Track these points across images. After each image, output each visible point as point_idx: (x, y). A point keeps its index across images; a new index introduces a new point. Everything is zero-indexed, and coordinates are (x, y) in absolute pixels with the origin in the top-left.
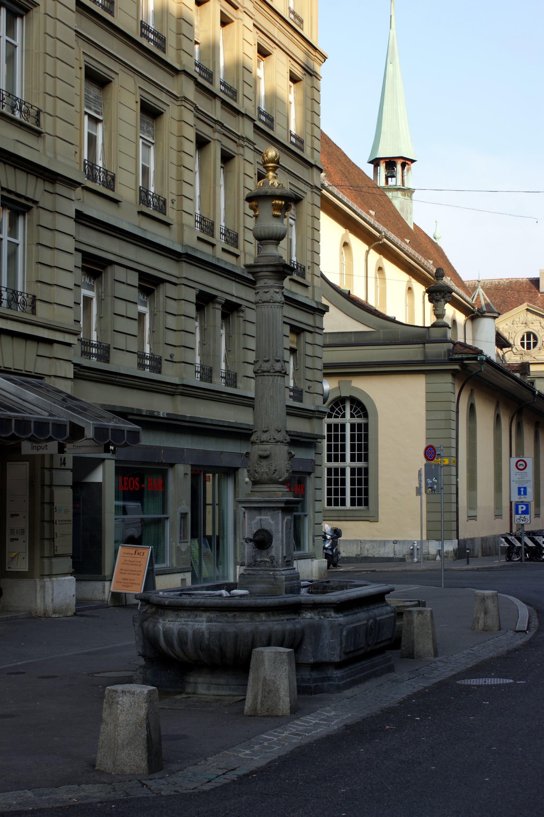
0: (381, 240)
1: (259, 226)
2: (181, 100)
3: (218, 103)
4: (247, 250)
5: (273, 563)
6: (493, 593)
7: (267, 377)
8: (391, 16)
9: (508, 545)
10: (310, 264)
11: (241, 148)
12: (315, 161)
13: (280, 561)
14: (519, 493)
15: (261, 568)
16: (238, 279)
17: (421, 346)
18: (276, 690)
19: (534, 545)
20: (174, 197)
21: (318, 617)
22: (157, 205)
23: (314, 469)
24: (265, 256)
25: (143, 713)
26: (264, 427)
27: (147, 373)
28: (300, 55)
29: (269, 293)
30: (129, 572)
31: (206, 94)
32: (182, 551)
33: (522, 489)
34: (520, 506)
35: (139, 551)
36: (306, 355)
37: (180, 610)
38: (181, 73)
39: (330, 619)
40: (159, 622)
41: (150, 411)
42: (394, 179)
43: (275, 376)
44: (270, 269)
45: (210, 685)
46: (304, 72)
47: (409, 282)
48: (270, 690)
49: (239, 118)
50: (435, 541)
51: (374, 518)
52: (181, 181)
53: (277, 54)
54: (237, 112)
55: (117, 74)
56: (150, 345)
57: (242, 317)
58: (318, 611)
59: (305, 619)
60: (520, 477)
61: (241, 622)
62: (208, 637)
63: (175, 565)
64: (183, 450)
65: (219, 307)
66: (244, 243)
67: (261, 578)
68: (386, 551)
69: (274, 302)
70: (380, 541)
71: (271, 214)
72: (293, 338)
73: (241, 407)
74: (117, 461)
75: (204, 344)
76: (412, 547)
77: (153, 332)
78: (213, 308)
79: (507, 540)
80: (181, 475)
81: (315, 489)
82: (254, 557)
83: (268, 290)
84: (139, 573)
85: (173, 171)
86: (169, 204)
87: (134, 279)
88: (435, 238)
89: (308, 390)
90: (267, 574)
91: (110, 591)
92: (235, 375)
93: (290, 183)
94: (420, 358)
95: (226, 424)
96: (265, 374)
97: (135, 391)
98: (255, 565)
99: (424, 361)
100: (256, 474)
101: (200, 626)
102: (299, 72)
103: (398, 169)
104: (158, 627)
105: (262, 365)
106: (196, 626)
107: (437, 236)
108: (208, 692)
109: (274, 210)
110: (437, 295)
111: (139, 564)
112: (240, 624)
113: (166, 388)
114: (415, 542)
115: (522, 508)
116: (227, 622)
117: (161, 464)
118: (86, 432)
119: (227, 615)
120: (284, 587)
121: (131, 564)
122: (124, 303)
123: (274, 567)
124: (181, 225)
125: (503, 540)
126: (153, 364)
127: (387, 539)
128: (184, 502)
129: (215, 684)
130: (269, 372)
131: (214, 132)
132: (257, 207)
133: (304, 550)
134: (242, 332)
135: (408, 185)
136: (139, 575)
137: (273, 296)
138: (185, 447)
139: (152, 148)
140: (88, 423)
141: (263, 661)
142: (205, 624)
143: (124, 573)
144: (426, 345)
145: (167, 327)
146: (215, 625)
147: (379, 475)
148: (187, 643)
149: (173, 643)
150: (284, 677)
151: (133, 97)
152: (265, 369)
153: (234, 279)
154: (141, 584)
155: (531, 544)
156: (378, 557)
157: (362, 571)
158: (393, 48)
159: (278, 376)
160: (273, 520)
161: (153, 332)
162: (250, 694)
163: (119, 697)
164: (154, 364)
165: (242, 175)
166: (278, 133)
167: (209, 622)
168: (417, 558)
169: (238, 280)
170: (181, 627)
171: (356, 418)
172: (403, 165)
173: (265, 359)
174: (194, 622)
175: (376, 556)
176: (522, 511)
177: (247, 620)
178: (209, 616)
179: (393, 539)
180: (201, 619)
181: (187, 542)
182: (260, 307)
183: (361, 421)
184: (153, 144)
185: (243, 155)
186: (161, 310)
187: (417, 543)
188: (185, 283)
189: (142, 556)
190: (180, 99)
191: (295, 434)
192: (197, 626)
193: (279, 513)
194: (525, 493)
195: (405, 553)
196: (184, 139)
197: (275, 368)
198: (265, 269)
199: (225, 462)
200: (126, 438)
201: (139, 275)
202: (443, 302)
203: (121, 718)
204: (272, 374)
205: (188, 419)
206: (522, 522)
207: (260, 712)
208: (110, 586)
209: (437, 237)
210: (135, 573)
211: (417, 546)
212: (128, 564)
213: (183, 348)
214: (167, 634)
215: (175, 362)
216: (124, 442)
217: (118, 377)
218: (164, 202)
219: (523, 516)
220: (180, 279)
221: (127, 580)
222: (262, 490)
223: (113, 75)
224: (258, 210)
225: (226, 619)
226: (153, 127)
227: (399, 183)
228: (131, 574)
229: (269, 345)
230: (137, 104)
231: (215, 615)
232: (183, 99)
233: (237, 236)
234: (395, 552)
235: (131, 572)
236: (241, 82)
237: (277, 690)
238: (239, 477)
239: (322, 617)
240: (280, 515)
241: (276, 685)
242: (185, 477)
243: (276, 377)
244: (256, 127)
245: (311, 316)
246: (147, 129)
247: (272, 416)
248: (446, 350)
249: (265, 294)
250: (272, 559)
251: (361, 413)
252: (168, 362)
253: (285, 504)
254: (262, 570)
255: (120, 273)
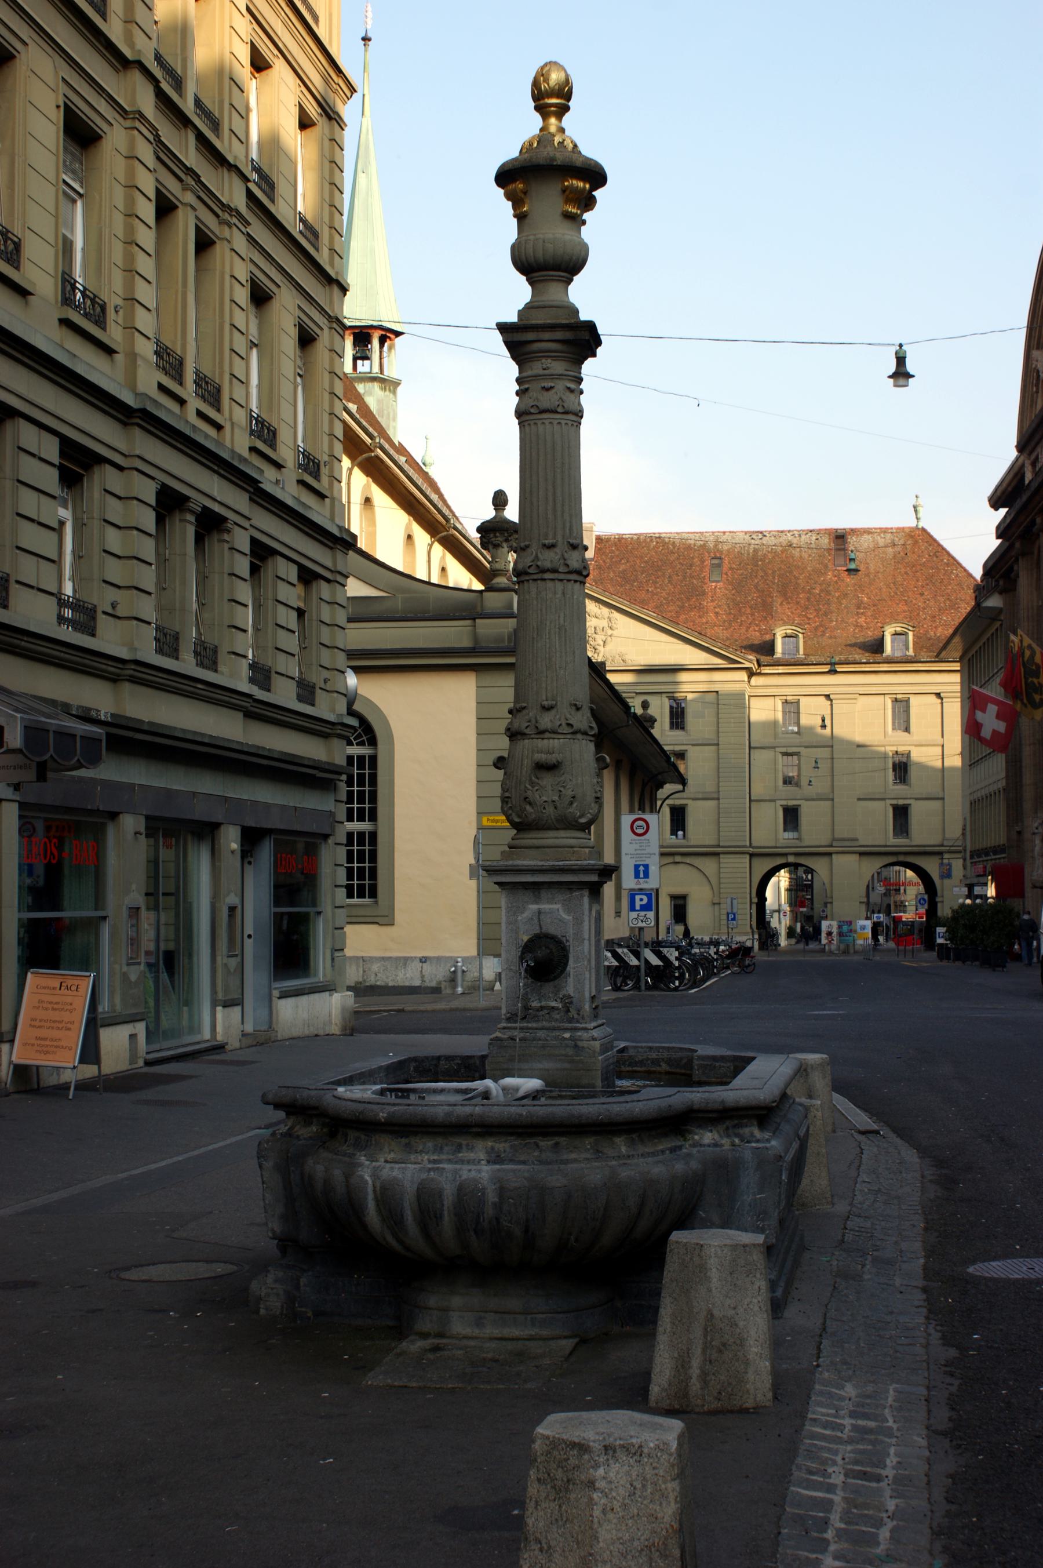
0: (372, 451)
1: (532, 237)
2: (133, 118)
3: (192, 137)
4: (235, 419)
5: (568, 1011)
6: (822, 1059)
7: (550, 584)
8: (364, 95)
9: (617, 964)
10: (326, 458)
11: (226, 228)
12: (337, 273)
13: (587, 1007)
14: (637, 875)
15: (540, 1025)
16: (224, 470)
17: (468, 622)
18: (738, 1342)
19: (660, 963)
20: (119, 302)
21: (729, 1140)
22: (92, 312)
23: (333, 829)
24: (545, 307)
25: (669, 1511)
26: (544, 698)
27: (67, 634)
28: (316, 79)
29: (553, 391)
30: (48, 1024)
31: (171, 116)
32: (131, 982)
33: (641, 868)
34: (637, 898)
35: (69, 982)
36: (321, 621)
37: (416, 1134)
38: (132, 66)
39: (754, 1145)
40: (361, 1165)
41: (83, 707)
42: (367, 363)
43: (569, 580)
44: (559, 335)
45: (482, 1314)
46: (319, 110)
47: (408, 527)
48: (724, 1345)
49: (223, 172)
50: (492, 957)
51: (387, 920)
52: (131, 271)
53: (279, 66)
54: (219, 160)
55: (25, 44)
56: (73, 582)
57: (228, 542)
58: (725, 1126)
59: (701, 1145)
60: (637, 847)
61: (575, 1161)
62: (496, 1200)
63: (118, 1008)
64: (131, 787)
65: (191, 518)
66: (230, 403)
67: (543, 1047)
68: (408, 975)
69: (566, 413)
70: (398, 959)
71: (559, 212)
72: (300, 589)
73: (225, 710)
74: (22, 806)
75: (164, 589)
76: (453, 969)
77: (80, 557)
78: (181, 521)
79: (616, 955)
80: (130, 836)
81: (336, 865)
82: (526, 999)
83: (553, 385)
84: (69, 1026)
85: (117, 252)
86: (111, 314)
87: (51, 449)
88: (424, 464)
89: (323, 686)
90: (556, 1038)
91: (10, 1062)
92: (215, 650)
93: (299, 307)
94: (466, 643)
95: (206, 740)
96: (547, 576)
97: (52, 670)
98: (525, 1018)
99: (474, 648)
100: (528, 807)
101: (473, 1174)
102: (313, 110)
103: (374, 346)
104: (362, 1177)
105: (539, 555)
106: (465, 1175)
107: (428, 461)
108: (477, 1332)
109: (567, 201)
110: (496, 537)
111: (69, 1007)
112: (575, 1166)
113: (104, 667)
114: (459, 960)
115: (641, 900)
116: (541, 1162)
117: (95, 812)
118: (7, 736)
119: (537, 1145)
120: (599, 1066)
121: (53, 1009)
122: (35, 494)
123: (571, 1020)
124: (133, 357)
125: (609, 954)
126: (82, 619)
127: (409, 955)
128: (134, 887)
129: (496, 1312)
130: (555, 571)
131: (184, 190)
132: (525, 193)
133: (316, 975)
134: (227, 570)
135: (390, 372)
136: (69, 1029)
137: (564, 398)
138: (137, 782)
139: (79, 204)
140: (13, 716)
141: (703, 1268)
142: (485, 1168)
143: (40, 1027)
144: (477, 620)
145: (106, 548)
146: (514, 1171)
147: (396, 845)
148: (441, 1216)
149: (402, 1216)
150: (756, 1308)
151: (52, 95)
152: (548, 565)
153: (216, 468)
154: (74, 1047)
155: (655, 961)
156: (394, 987)
157: (381, 1011)
158: (367, 147)
159: (576, 581)
160: (568, 911)
161: (80, 557)
162: (666, 1355)
163: (596, 1466)
164: (81, 618)
165: (227, 278)
166: (281, 211)
167: (495, 1163)
168: (462, 987)
169: (222, 472)
170: (424, 1176)
171: (355, 747)
172: (383, 340)
173: (547, 542)
174: (456, 1163)
175: (390, 985)
176: (641, 906)
177: (588, 1156)
178: (493, 1148)
179: (420, 955)
180: (472, 1156)
181: (139, 964)
182: (532, 422)
183: (365, 751)
184: (81, 195)
185: (229, 242)
186: (95, 515)
187: (463, 961)
188: (140, 467)
189: (75, 993)
190: (131, 116)
191: (311, 763)
192: (467, 1173)
193: (582, 896)
194: (646, 875)
195: (441, 979)
196: (138, 193)
197: (569, 562)
198: (547, 336)
199: (200, 812)
200: (78, 752)
201: (60, 444)
202: (506, 549)
203: (606, 1533)
204: (562, 577)
205: (146, 728)
206: (640, 924)
207: (699, 1402)
208: (11, 1053)
209: (427, 462)
210: (60, 1026)
211: (463, 966)
212: (47, 1009)
213: (135, 592)
214: (387, 1195)
215: (119, 618)
216: (76, 759)
217: (25, 639)
218: (103, 308)
219: (643, 913)
220: (129, 459)
221: (45, 1039)
222: (536, 842)
223: (18, 45)
224: (527, 201)
225: (536, 1154)
226: (82, 164)
227: (376, 369)
228: (53, 1028)
229: (555, 510)
230: (59, 111)
231: (507, 1145)
232: (137, 116)
233: (219, 390)
234: (423, 977)
235: (52, 1025)
236: (226, 106)
237: (741, 1343)
238: (222, 841)
239: (737, 1141)
240: (586, 900)
241: (738, 1330)
242: (136, 839)
243: (570, 585)
244: (250, 194)
245: (328, 550)
246: (71, 165)
247: (562, 672)
248: (511, 630)
249: (545, 393)
250: (568, 1003)
251: (364, 738)
252: (107, 617)
253: (599, 875)
254: (542, 1029)
255: (28, 436)
